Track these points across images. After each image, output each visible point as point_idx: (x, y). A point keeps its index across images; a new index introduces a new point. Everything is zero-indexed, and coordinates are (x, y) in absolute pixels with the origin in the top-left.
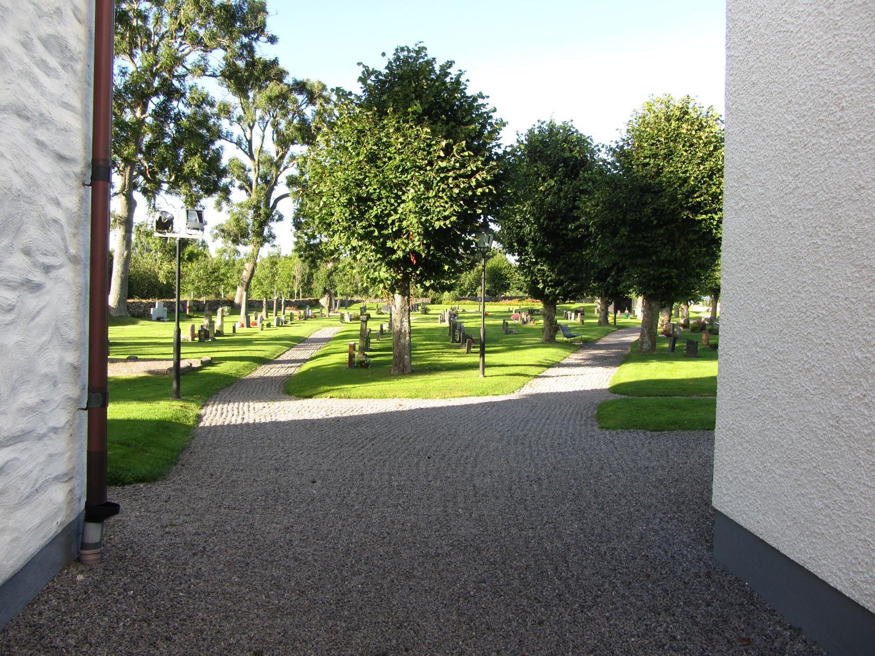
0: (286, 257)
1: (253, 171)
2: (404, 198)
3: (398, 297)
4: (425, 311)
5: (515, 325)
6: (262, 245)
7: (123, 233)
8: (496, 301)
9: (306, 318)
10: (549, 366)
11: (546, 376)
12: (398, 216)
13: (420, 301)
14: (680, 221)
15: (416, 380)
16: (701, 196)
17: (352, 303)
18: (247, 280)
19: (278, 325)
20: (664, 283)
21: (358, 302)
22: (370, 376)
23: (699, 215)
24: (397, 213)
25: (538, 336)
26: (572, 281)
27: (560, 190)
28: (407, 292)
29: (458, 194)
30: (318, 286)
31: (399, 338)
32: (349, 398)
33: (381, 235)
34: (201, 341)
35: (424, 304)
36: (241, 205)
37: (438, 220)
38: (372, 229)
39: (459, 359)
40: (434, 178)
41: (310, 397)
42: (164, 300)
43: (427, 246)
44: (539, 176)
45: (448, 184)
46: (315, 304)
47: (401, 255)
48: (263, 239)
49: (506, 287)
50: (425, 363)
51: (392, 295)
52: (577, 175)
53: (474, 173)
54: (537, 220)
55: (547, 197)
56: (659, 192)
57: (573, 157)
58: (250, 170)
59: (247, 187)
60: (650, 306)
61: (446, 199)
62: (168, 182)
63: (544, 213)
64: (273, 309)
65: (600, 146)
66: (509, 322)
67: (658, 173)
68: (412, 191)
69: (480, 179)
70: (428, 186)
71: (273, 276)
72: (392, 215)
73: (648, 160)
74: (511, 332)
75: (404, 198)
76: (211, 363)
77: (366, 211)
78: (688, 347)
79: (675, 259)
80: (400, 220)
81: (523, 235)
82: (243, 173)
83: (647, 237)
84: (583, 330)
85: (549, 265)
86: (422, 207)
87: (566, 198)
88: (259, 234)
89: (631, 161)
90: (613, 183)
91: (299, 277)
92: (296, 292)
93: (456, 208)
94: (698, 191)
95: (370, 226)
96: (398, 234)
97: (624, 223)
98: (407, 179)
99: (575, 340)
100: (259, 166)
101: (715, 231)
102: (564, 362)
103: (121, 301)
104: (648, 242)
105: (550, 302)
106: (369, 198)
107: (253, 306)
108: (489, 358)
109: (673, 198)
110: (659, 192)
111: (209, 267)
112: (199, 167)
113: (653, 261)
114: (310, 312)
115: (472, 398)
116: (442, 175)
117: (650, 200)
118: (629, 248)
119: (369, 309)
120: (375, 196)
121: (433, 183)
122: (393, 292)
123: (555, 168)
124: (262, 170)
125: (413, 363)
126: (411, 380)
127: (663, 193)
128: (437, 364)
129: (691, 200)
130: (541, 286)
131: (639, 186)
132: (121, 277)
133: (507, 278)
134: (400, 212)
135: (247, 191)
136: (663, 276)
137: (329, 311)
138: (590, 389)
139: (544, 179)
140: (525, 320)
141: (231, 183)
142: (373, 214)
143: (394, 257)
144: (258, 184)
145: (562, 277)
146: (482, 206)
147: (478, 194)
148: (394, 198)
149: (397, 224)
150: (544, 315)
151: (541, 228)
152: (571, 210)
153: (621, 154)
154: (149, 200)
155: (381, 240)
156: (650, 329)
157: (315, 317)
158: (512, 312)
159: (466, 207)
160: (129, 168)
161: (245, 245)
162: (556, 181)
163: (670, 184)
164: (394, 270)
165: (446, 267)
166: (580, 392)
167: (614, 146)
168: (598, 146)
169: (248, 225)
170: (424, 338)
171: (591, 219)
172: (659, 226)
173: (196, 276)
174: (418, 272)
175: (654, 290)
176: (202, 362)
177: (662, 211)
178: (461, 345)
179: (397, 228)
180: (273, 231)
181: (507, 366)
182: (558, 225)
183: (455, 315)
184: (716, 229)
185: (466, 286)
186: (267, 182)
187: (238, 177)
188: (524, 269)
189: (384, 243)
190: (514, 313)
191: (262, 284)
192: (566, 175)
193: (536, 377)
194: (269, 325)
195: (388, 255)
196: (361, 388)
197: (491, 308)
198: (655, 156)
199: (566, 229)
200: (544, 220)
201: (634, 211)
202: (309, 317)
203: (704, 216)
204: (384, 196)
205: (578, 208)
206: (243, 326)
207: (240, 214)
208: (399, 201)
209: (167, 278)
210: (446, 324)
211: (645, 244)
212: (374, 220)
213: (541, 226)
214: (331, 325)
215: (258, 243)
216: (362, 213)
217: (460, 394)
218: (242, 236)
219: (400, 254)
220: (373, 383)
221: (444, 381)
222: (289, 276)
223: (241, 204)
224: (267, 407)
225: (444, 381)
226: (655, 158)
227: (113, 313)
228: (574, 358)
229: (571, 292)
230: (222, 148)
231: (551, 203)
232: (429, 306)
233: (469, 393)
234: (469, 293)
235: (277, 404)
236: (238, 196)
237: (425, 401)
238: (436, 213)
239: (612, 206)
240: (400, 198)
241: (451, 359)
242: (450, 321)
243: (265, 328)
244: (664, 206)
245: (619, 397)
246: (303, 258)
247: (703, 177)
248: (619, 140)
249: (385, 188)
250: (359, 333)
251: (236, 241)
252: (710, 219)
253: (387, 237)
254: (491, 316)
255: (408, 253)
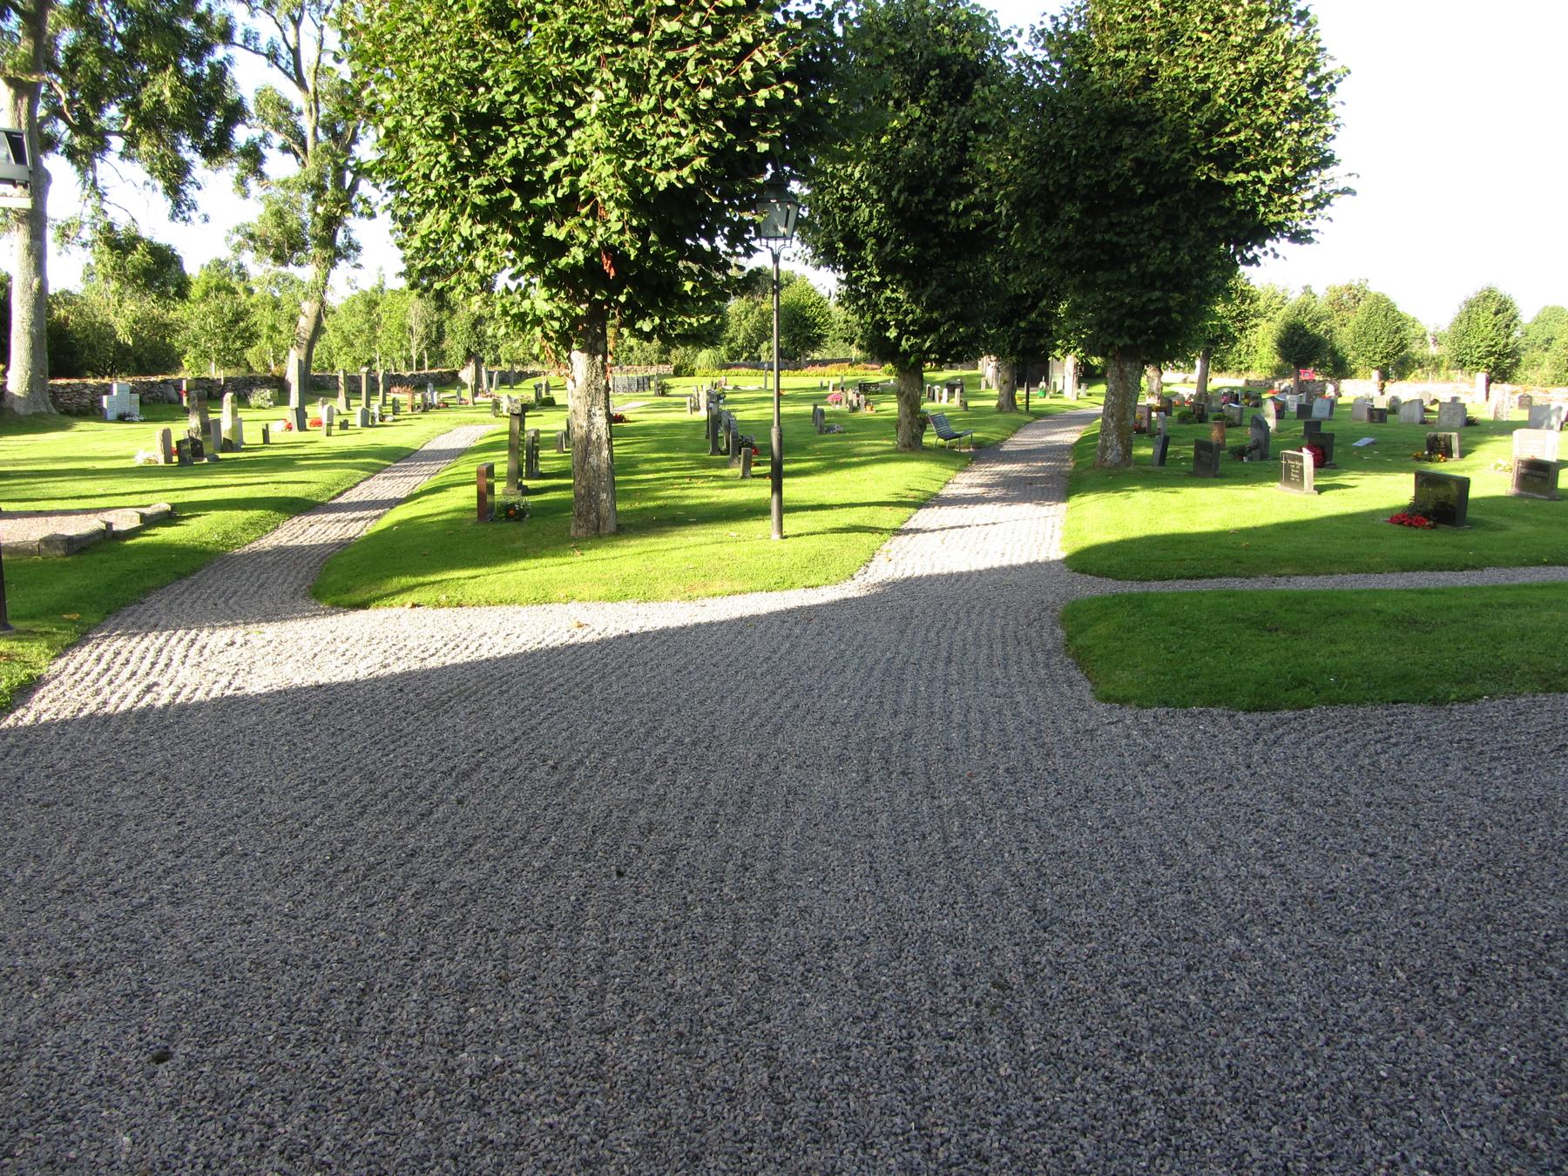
0: (394, 292)
1: (306, 113)
2: (579, 114)
3: (579, 359)
4: (663, 391)
5: (835, 414)
6: (334, 265)
7: (27, 241)
8: (796, 369)
9: (427, 407)
10: (919, 505)
11: (917, 531)
12: (567, 160)
13: (653, 371)
14: (1193, 186)
15: (625, 551)
16: (1237, 131)
17: (522, 376)
18: (307, 336)
19: (365, 424)
20: (1152, 323)
21: (535, 374)
22: (519, 544)
23: (1231, 174)
24: (564, 153)
25: (885, 436)
26: (957, 323)
27: (933, 128)
28: (600, 346)
29: (710, 102)
30: (455, 346)
31: (586, 454)
32: (460, 605)
33: (530, 210)
34: (183, 462)
35: (660, 376)
36: (284, 184)
37: (666, 167)
38: (506, 193)
39: (726, 491)
40: (651, 62)
41: (364, 605)
42: (137, 379)
43: (642, 233)
44: (889, 97)
45: (685, 78)
46: (450, 380)
47: (581, 258)
48: (335, 250)
49: (816, 342)
50: (651, 504)
51: (566, 355)
52: (969, 90)
53: (747, 49)
54: (886, 191)
55: (905, 143)
56: (1148, 123)
57: (959, 55)
58: (300, 113)
59: (296, 147)
60: (1122, 371)
61: (683, 116)
62: (120, 134)
63: (898, 178)
64: (360, 392)
65: (1015, 32)
66: (826, 408)
67: (1148, 80)
68: (599, 95)
69: (764, 64)
70: (638, 84)
71: (372, 328)
72: (553, 159)
73: (1122, 54)
74: (830, 429)
75: (579, 114)
76: (171, 517)
77: (490, 150)
78: (1197, 454)
79: (1178, 270)
80: (575, 171)
81: (856, 226)
82: (286, 117)
83: (1120, 224)
84: (971, 423)
85: (908, 288)
86: (622, 137)
87: (944, 143)
88: (327, 242)
89: (1088, 56)
90: (1048, 105)
91: (420, 330)
92: (415, 358)
93: (706, 137)
94: (1230, 121)
95: (500, 185)
96: (568, 206)
97: (1071, 193)
98: (585, 69)
99: (960, 443)
100: (316, 101)
101: (1262, 209)
102: (948, 492)
103: (34, 383)
104: (1118, 234)
105: (910, 368)
106: (494, 116)
107: (317, 386)
108: (794, 489)
109: (1180, 137)
110: (1148, 123)
111: (226, 310)
112: (174, 95)
113: (1130, 276)
114: (436, 397)
115: (751, 598)
116: (671, 55)
117: (1128, 140)
118: (1080, 248)
119: (556, 388)
120: (509, 112)
121: (649, 76)
122: (569, 350)
123: (923, 78)
124: (324, 111)
125: (620, 507)
126: (614, 552)
127: (1156, 127)
128: (677, 507)
129: (1216, 140)
130: (892, 333)
131: (1106, 110)
132: (30, 333)
133: (816, 325)
134: (571, 149)
135: (297, 156)
136: (1152, 307)
137: (475, 394)
138: (1022, 561)
139: (899, 105)
140: (855, 404)
141: (263, 139)
142: (508, 156)
143: (563, 262)
144: (317, 141)
145: (935, 315)
146: (769, 135)
147: (760, 103)
148: (555, 115)
149: (566, 181)
150: (900, 394)
151: (893, 210)
152: (956, 170)
153: (1060, 41)
154: (82, 170)
155: (531, 221)
156: (1119, 420)
157: (446, 405)
158: (826, 388)
159: (730, 136)
160: (26, 100)
161: (299, 264)
162: (923, 109)
163: (1173, 104)
164: (567, 293)
165: (688, 286)
166: (1004, 571)
167: (1049, 26)
168: (1009, 31)
169: (303, 225)
170: (655, 445)
171: (1001, 185)
172: (1147, 199)
173: (202, 328)
174: (622, 299)
175: (1132, 337)
176: (143, 517)
177: (1155, 164)
178: (731, 461)
179: (566, 190)
180: (352, 235)
181: (830, 507)
182: (928, 203)
183: (719, 397)
184: (1265, 205)
185: (740, 342)
186: (336, 137)
187: (277, 126)
188: (857, 298)
189: (537, 230)
190: (830, 391)
191: (352, 345)
192: (944, 95)
193: (897, 532)
194: (344, 425)
195: (549, 258)
196: (490, 578)
197: (792, 381)
198: (1139, 44)
199: (945, 211)
200: (900, 192)
201: (1094, 167)
202: (432, 406)
203: (1242, 177)
204: (530, 110)
205: (972, 163)
206: (289, 428)
207: (285, 202)
208: (569, 123)
209: (133, 333)
210: (702, 415)
211: (1115, 239)
212: (510, 171)
213: (892, 207)
214: (473, 422)
215: (324, 260)
216: (481, 154)
217: (728, 587)
218: (293, 247)
219: (577, 254)
220: (523, 564)
221: (689, 553)
222: (402, 326)
223: (286, 182)
224: (239, 640)
225: (689, 553)
226: (1139, 48)
227: (20, 409)
228: (965, 482)
229: (954, 344)
230: (229, 60)
231: (913, 157)
232: (669, 381)
233: (750, 584)
234: (745, 355)
235: (271, 630)
236: (280, 165)
237: (643, 609)
238: (659, 151)
239: (1044, 156)
240: (572, 117)
241: (709, 492)
242: (709, 409)
243: (336, 430)
244: (1158, 153)
245: (1109, 587)
246: (418, 290)
247: (1243, 90)
248: (1057, 12)
249: (533, 90)
250: (506, 437)
251: (280, 258)
252: (1254, 183)
253: (546, 214)
254: (788, 398)
255: (597, 253)
